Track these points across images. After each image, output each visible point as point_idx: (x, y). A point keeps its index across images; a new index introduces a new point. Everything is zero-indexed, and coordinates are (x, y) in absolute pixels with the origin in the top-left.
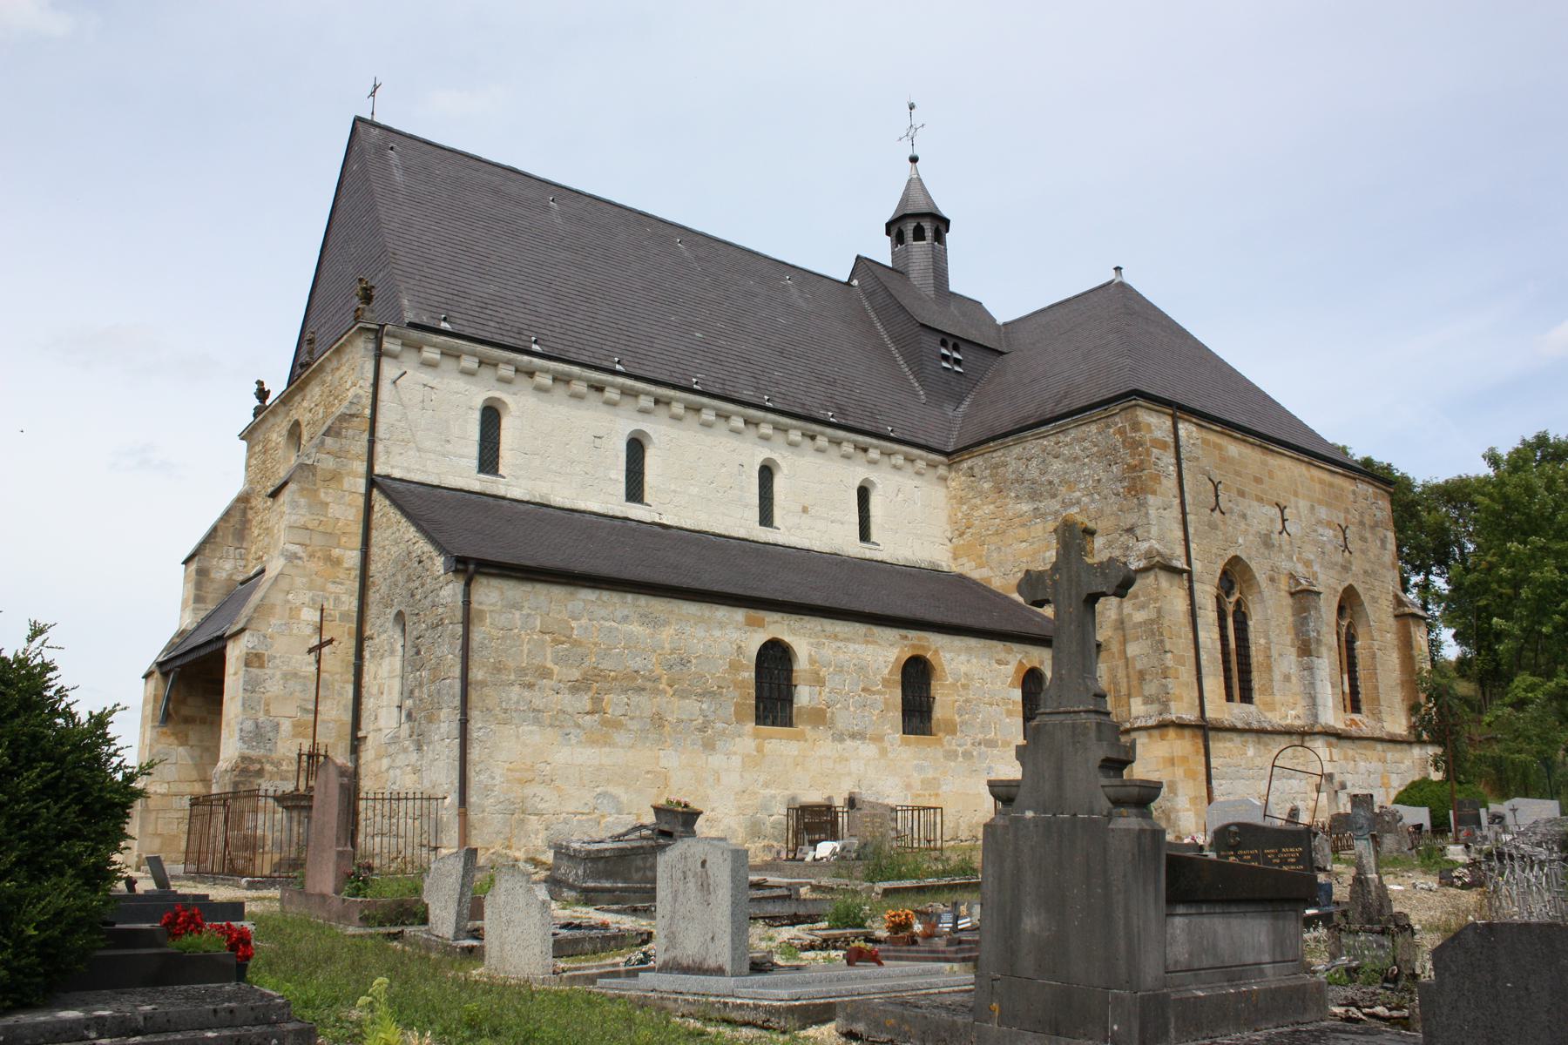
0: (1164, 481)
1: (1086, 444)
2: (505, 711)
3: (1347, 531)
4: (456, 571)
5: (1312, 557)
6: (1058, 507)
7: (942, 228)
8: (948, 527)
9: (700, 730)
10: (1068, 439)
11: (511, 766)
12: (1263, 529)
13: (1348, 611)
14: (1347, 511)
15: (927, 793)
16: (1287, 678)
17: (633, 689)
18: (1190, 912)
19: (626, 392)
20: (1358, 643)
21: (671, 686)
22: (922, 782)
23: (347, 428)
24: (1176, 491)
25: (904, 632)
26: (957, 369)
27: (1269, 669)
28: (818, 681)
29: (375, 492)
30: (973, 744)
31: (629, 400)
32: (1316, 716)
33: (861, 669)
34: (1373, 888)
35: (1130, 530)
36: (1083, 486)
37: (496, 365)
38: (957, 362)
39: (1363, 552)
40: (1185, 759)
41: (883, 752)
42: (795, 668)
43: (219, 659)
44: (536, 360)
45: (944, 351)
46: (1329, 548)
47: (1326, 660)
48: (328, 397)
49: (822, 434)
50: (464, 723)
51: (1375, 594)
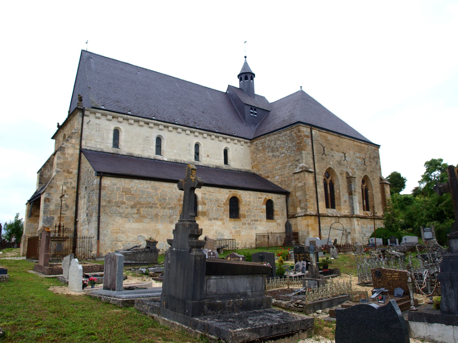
0: (307, 146)
1: (286, 136)
2: (111, 214)
3: (365, 160)
4: (97, 175)
5: (354, 167)
6: (279, 154)
7: (253, 76)
8: (251, 160)
9: (169, 218)
10: (281, 135)
11: (113, 229)
12: (338, 159)
13: (366, 182)
14: (365, 154)
15: (236, 235)
16: (345, 201)
17: (149, 207)
18: (217, 278)
19: (155, 124)
20: (369, 191)
21: (160, 206)
22: (235, 231)
23: (74, 136)
24: (311, 149)
25: (230, 190)
26: (255, 116)
27: (340, 199)
28: (204, 204)
29: (82, 154)
30: (251, 221)
31: (156, 127)
32: (353, 212)
33: (217, 200)
34: (314, 268)
35: (298, 160)
36: (285, 148)
37: (117, 118)
38: (255, 114)
39: (370, 165)
40: (312, 225)
41: (224, 223)
42: (198, 200)
43: (40, 198)
44: (129, 116)
45: (252, 111)
46: (359, 164)
47: (357, 197)
48: (284, 113)
49: (213, 135)
50: (99, 217)
51: (374, 177)
